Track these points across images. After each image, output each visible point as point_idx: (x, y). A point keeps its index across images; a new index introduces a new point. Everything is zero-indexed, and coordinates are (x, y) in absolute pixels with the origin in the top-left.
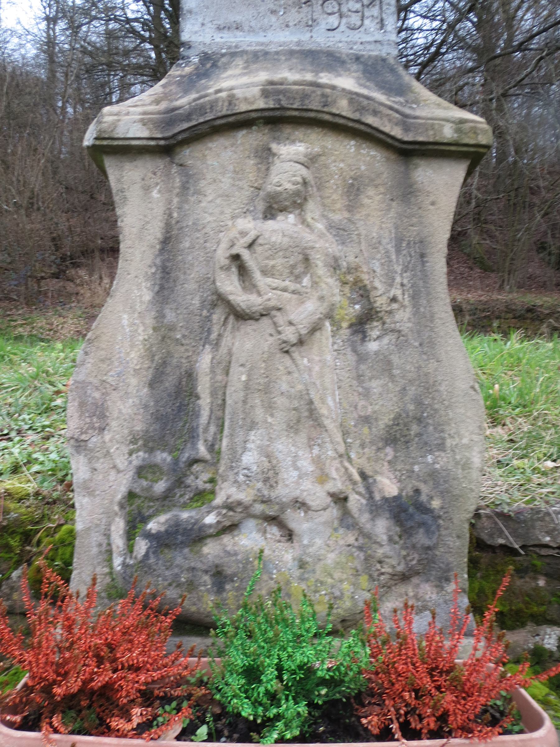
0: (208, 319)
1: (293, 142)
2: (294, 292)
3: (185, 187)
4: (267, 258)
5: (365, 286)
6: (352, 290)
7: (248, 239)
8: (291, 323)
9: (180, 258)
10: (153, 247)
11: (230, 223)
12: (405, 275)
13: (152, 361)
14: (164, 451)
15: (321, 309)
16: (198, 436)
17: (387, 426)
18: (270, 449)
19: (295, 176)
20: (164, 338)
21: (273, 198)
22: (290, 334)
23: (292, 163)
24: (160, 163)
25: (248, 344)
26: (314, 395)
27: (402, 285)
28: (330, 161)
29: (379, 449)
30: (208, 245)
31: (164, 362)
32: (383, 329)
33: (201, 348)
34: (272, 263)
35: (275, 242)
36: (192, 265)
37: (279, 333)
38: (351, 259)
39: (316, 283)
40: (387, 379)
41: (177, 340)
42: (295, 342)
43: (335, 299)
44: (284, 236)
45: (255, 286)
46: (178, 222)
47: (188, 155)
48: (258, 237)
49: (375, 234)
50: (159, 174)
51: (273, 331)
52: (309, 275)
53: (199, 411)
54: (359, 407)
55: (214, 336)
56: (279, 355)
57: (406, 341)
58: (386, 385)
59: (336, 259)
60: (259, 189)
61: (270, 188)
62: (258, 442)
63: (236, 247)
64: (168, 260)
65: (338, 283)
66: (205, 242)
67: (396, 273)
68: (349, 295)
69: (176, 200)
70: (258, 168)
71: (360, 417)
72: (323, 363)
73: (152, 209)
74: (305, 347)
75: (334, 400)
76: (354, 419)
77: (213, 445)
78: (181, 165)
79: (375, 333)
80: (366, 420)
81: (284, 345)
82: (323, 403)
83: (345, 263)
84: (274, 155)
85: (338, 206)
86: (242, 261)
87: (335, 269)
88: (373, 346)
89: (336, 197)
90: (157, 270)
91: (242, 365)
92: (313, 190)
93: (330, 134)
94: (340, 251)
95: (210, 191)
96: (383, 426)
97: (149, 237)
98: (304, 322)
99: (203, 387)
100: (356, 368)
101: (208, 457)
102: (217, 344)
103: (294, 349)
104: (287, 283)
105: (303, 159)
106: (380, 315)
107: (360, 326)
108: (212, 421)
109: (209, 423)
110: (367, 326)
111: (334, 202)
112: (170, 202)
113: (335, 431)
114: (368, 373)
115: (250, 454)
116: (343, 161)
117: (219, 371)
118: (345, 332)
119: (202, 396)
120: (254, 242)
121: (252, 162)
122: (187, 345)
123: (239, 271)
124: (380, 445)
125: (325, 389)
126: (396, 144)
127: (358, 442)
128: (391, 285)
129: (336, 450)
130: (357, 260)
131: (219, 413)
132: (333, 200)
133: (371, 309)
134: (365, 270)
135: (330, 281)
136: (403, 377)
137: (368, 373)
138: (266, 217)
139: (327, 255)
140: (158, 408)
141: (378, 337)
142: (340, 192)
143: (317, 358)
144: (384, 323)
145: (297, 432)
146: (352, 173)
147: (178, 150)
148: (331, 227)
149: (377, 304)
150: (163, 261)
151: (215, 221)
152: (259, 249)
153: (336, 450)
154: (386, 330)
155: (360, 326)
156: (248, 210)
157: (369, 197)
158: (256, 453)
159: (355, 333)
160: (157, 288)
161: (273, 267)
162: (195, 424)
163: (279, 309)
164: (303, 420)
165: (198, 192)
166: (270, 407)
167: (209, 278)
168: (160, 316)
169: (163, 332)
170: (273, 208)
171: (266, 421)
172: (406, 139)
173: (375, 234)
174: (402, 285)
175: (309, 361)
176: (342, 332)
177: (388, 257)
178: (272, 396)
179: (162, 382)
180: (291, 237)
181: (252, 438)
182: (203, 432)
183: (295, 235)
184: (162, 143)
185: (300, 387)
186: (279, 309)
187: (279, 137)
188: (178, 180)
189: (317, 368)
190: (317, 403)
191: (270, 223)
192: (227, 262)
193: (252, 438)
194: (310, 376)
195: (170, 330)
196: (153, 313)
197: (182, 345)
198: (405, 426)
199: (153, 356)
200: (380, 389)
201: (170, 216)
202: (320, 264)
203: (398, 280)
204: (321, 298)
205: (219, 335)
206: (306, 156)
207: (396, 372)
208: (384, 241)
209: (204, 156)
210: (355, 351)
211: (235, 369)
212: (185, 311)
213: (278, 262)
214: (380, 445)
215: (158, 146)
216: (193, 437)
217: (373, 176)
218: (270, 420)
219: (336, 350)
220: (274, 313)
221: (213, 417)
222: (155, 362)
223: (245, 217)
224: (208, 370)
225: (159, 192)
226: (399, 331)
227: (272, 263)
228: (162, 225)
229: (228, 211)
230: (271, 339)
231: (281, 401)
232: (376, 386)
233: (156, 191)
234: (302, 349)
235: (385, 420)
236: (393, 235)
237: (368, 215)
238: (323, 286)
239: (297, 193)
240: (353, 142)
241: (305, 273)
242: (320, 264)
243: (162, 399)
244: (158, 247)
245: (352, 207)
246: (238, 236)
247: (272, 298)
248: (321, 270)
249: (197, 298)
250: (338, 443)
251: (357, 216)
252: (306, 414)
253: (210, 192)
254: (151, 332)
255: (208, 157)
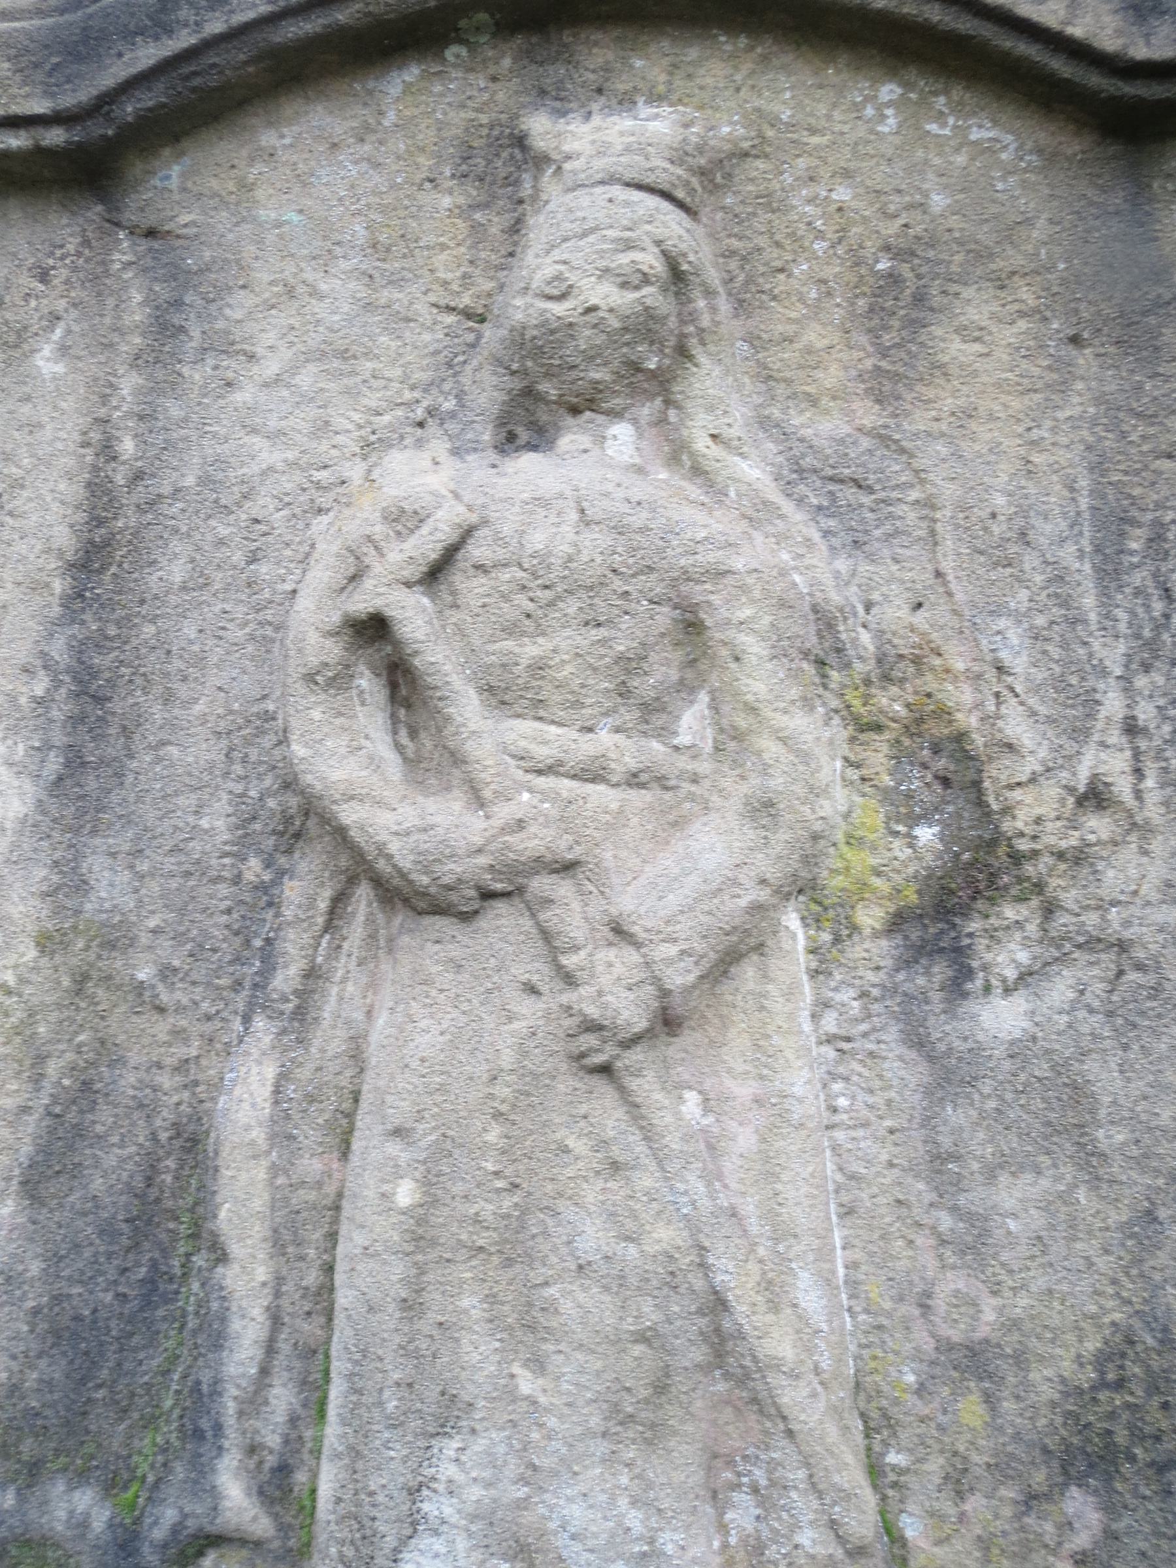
0: (267, 895)
1: (626, 102)
2: (634, 780)
3: (165, 327)
4: (511, 630)
5: (960, 737)
6: (899, 755)
7: (425, 545)
8: (620, 932)
9: (149, 630)
10: (38, 587)
11: (355, 472)
12: (1141, 682)
13: (37, 1080)
14: (81, 1477)
15: (764, 865)
16: (218, 1428)
17: (1071, 1391)
18: (527, 1518)
19: (629, 246)
20: (81, 980)
21: (538, 352)
22: (615, 989)
23: (617, 191)
24: (64, 229)
25: (429, 1024)
26: (732, 1274)
27: (1131, 728)
28: (788, 179)
29: (1031, 1500)
30: (264, 569)
31: (86, 1086)
32: (1045, 938)
33: (237, 1025)
34: (530, 650)
35: (543, 557)
36: (200, 661)
37: (569, 979)
38: (895, 613)
39: (738, 736)
40: (1068, 1171)
41: (140, 988)
42: (641, 1025)
43: (826, 808)
44: (585, 520)
45: (457, 759)
46: (138, 476)
47: (178, 187)
48: (468, 533)
49: (1000, 500)
50: (60, 275)
51: (537, 971)
52: (703, 697)
53: (223, 1320)
54: (940, 1303)
55: (286, 978)
56: (567, 1083)
57: (1156, 991)
58: (1066, 1198)
59: (826, 621)
60: (482, 320)
61: (522, 309)
62: (475, 1493)
63: (368, 583)
64: (101, 642)
65: (839, 731)
66: (253, 559)
67: (1104, 673)
68: (887, 781)
69: (129, 383)
70: (475, 227)
71: (945, 1346)
72: (773, 1107)
73: (34, 427)
74: (688, 1039)
75: (828, 1281)
76: (917, 1355)
77: (283, 1470)
78: (151, 233)
79: (1009, 956)
80: (972, 1362)
81: (590, 1040)
82: (774, 1307)
83: (865, 637)
84: (541, 161)
85: (831, 376)
86: (397, 644)
87: (821, 663)
88: (1001, 1018)
89: (823, 338)
90: (57, 684)
91: (398, 1132)
92: (715, 311)
93: (787, 58)
94: (842, 582)
95: (270, 338)
96: (1048, 1392)
97: (21, 547)
98: (682, 928)
99: (242, 1202)
100: (926, 1122)
101: (262, 1525)
102: (300, 1014)
103: (634, 1056)
104: (605, 738)
105: (665, 172)
106: (1029, 869)
107: (941, 921)
108: (280, 1361)
109: (264, 1371)
110: (975, 925)
111: (812, 360)
112: (105, 392)
113: (832, 1432)
114: (979, 1145)
115: (439, 1545)
116: (847, 174)
117: (309, 1135)
118: (872, 952)
119: (235, 1249)
120: (449, 556)
121: (447, 201)
122: (180, 1009)
123: (393, 686)
124: (1039, 1478)
125: (781, 1233)
126: (1095, 80)
127: (935, 1465)
128: (1080, 733)
129: (833, 1524)
130: (920, 619)
131: (311, 1329)
132: (809, 350)
133: (992, 844)
134: (960, 665)
135: (799, 723)
136: (1142, 1162)
137: (979, 1145)
138: (511, 437)
139: (782, 604)
140: (62, 1286)
141: (1025, 977)
142: (838, 314)
143: (743, 1091)
144: (1049, 910)
145: (654, 1435)
146: (891, 229)
147: (137, 168)
148: (797, 472)
149: (1021, 821)
150: (79, 649)
151: (293, 465)
152: (470, 587)
153: (833, 1524)
154: (1057, 943)
155: (941, 921)
156: (431, 412)
157: (967, 333)
158: (462, 1544)
159: (916, 955)
160: (54, 764)
161: (538, 667)
162: (206, 1377)
163: (567, 868)
164: (681, 1385)
165: (225, 346)
166: (528, 1329)
167: (269, 717)
168: (70, 883)
169: (84, 949)
170: (537, 402)
171: (512, 1395)
172: (1141, 52)
173: (1000, 500)
174: (1131, 728)
175: (707, 1105)
176: (857, 951)
177: (1065, 602)
178: (537, 1276)
179: (75, 1171)
180: (620, 530)
181: (448, 1470)
182: (241, 1414)
183: (639, 519)
184: (55, 137)
185: (665, 1235)
186: (567, 868)
187: (560, 85)
188: (138, 298)
189: (745, 1140)
190: (746, 1310)
191: (528, 466)
192: (334, 650)
193: (448, 1470)
194: (712, 1177)
195: (111, 945)
196: (40, 873)
197: (161, 1010)
198: (1153, 1389)
199: (41, 1059)
200: (1038, 1220)
201: (107, 451)
202: (753, 646)
203: (1113, 704)
204: (763, 810)
205: (312, 973)
206: (679, 156)
207: (1112, 1138)
208: (1045, 530)
209: (246, 187)
210: (917, 1040)
211: (368, 1137)
212: (170, 864)
213: (562, 644)
214: (1039, 1478)
215: (39, 152)
216: (198, 1435)
217: (985, 235)
218: (527, 1384)
219: (830, 1039)
220: (540, 884)
221: (284, 1347)
222: (48, 1087)
223: (420, 443)
224: (259, 1135)
225: (63, 350)
226: (1122, 946)
227: (530, 650)
228: (74, 491)
229: (347, 418)
230: (529, 1010)
231: (575, 1304)
232: (1016, 1203)
233: (47, 350)
234: (675, 1049)
235: (1060, 1365)
236: (1084, 502)
237: (969, 413)
238: (771, 748)
239: (643, 327)
240: (889, 91)
241: (686, 688)
242: (753, 646)
243: (77, 1247)
244: (58, 586)
245: (896, 377)
246: (379, 530)
247: (531, 815)
248: (761, 677)
249: (222, 804)
250: (847, 1496)
251: (920, 421)
252: (699, 1354)
253: (272, 343)
254: (32, 953)
255: (260, 194)
